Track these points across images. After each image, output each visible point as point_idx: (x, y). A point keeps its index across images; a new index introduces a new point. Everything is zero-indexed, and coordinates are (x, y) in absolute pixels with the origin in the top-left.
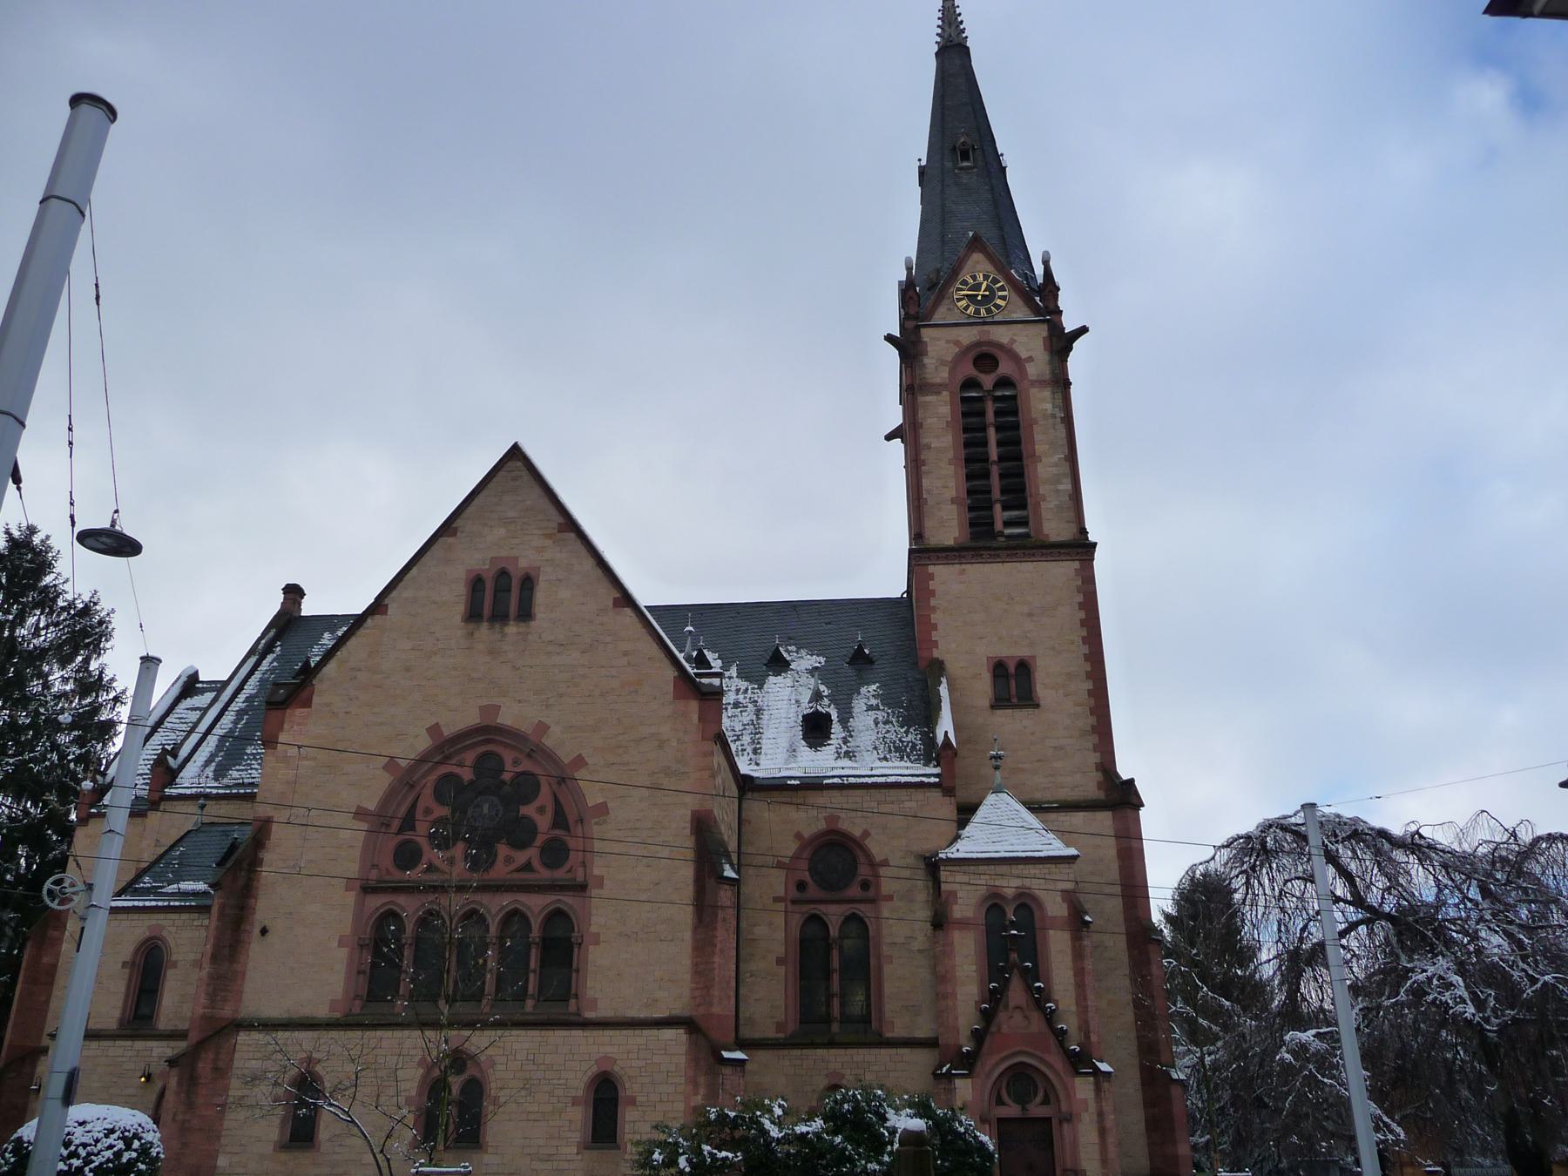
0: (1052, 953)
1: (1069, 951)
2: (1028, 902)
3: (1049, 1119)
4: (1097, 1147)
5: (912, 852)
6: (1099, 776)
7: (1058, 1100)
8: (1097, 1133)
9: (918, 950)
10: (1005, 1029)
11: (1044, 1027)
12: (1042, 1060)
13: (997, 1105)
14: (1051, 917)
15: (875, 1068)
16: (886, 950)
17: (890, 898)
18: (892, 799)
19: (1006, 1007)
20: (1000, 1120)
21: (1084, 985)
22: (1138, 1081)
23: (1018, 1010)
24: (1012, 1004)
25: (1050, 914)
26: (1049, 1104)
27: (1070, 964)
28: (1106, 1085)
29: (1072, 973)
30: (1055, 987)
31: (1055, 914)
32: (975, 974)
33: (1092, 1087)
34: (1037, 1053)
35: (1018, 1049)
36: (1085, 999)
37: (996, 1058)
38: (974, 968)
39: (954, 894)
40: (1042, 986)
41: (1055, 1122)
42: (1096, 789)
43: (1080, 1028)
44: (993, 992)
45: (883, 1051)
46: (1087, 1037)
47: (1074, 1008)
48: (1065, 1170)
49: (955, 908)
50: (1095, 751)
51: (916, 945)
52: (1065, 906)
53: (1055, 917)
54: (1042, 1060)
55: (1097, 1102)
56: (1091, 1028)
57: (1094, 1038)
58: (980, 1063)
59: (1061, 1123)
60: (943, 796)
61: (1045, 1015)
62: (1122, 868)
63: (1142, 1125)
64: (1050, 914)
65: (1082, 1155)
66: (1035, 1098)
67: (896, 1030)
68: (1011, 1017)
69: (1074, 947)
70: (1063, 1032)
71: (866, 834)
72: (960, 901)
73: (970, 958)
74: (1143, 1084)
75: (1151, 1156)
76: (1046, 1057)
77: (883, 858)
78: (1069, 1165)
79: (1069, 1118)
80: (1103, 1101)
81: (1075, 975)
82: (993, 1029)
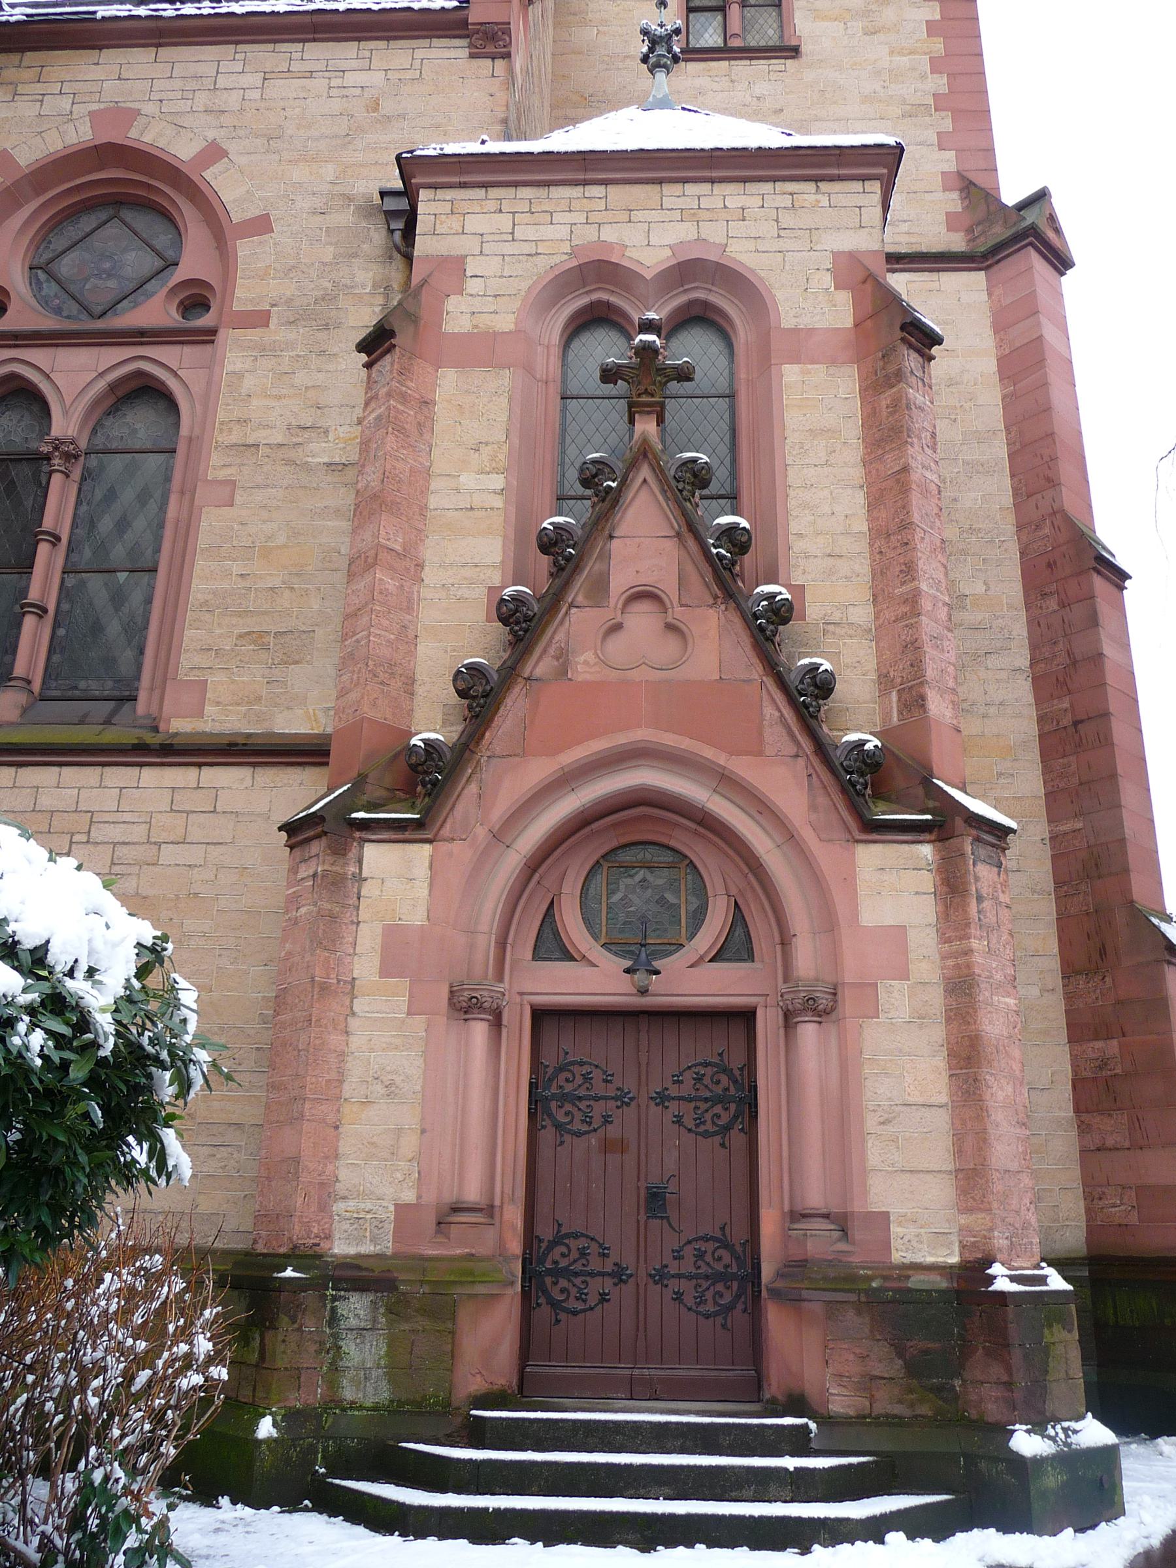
0: (792, 438)
1: (853, 431)
2: (717, 299)
3: (746, 1017)
4: (941, 1121)
5: (349, 198)
6: (953, 201)
7: (786, 941)
8: (940, 1062)
9: (328, 465)
10: (585, 666)
11: (751, 669)
12: (726, 781)
13: (536, 957)
14: (796, 331)
15: (115, 833)
16: (217, 465)
17: (260, 319)
18: (309, 66)
19: (601, 587)
20: (542, 1016)
21: (906, 526)
22: (1053, 964)
23: (644, 606)
24: (620, 582)
25: (787, 322)
26: (751, 958)
27: (857, 473)
28: (983, 875)
29: (860, 498)
30: (798, 546)
31: (805, 322)
32: (498, 502)
33: (927, 881)
34: (709, 753)
35: (622, 739)
36: (909, 571)
37: (539, 770)
38: (497, 481)
39: (456, 265)
40: (744, 523)
41: (767, 1024)
42: (943, 229)
43: (884, 681)
44: (550, 543)
45: (150, 776)
46: (914, 702)
47: (862, 614)
48: (797, 1216)
49: (453, 304)
50: (941, 148)
51: (320, 452)
52: (844, 299)
53: (811, 331)
54: (726, 781)
55: (944, 939)
56: (930, 673)
57: (938, 706)
58: (473, 788)
59: (789, 1020)
60: (472, 56)
61: (749, 619)
62: (1009, 401)
63: (1064, 1093)
64: (788, 321)
65: (875, 1154)
66: (692, 936)
67: (209, 709)
68: (617, 627)
69: (870, 419)
70: (822, 685)
71: (214, 153)
72: (473, 286)
73: (486, 450)
74: (1069, 971)
75: (1093, 1192)
76: (742, 767)
77: (253, 212)
78: (815, 1197)
79: (824, 1002)
80: (974, 931)
81: (873, 504)
82: (540, 665)
